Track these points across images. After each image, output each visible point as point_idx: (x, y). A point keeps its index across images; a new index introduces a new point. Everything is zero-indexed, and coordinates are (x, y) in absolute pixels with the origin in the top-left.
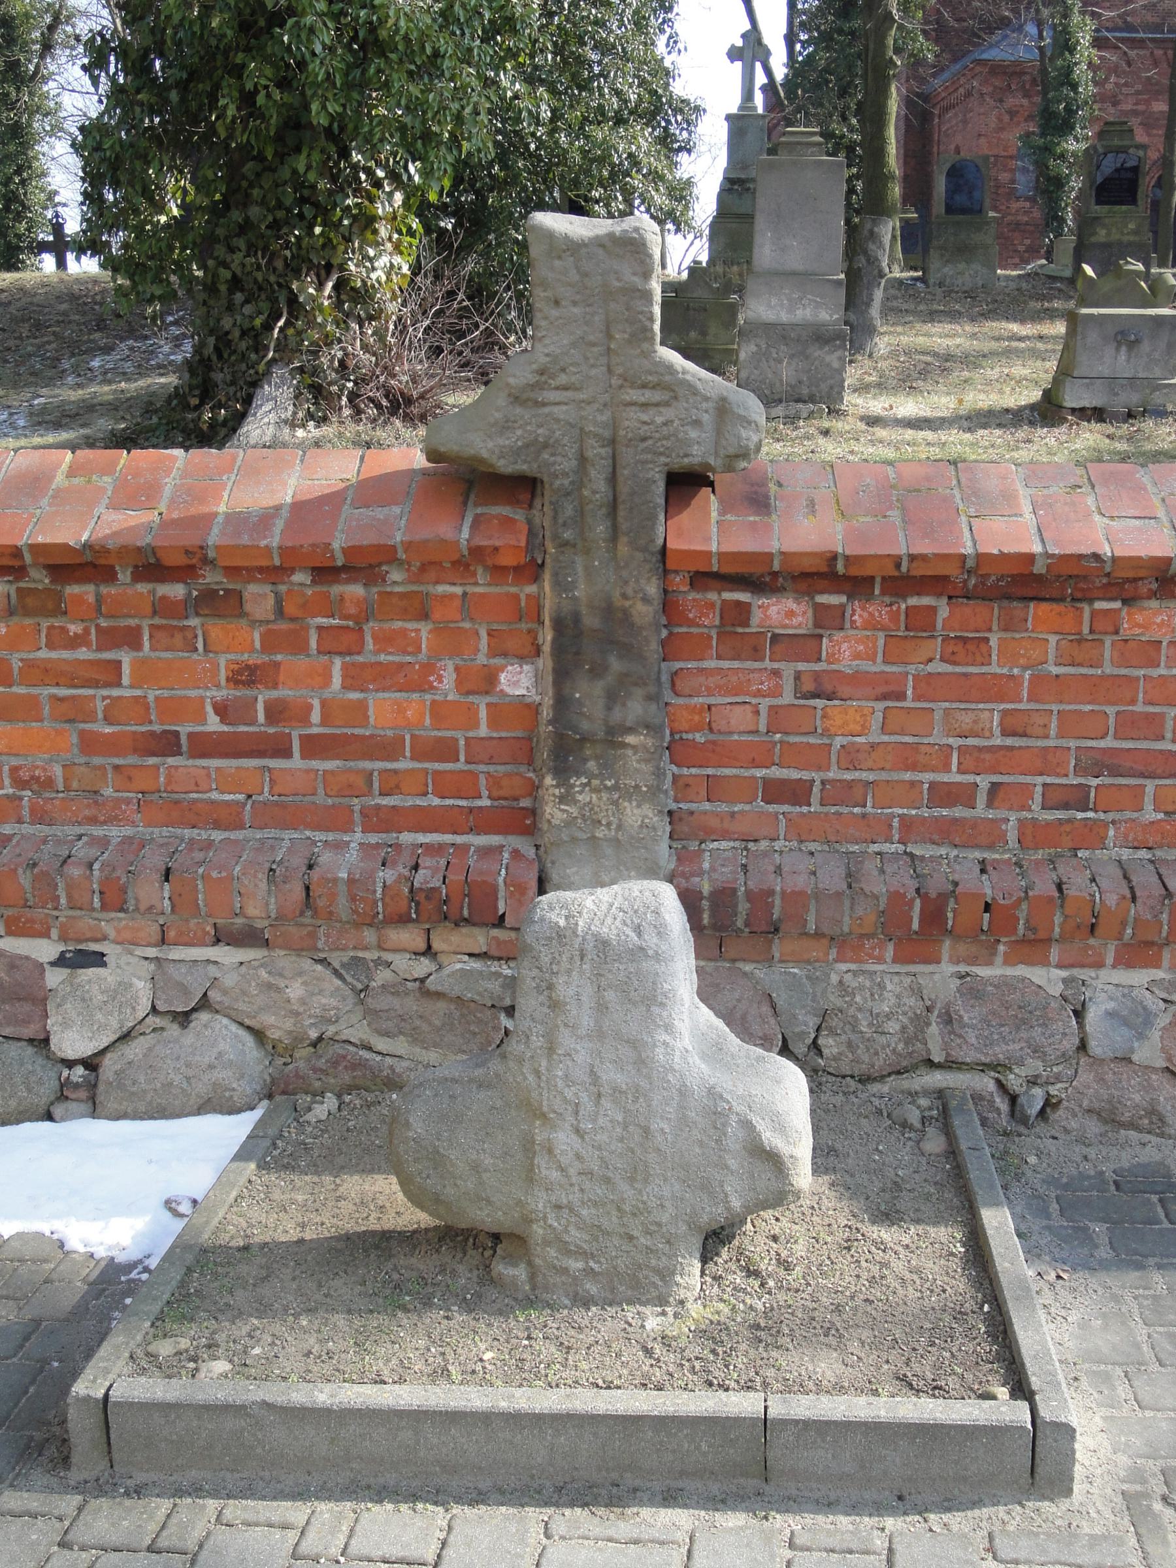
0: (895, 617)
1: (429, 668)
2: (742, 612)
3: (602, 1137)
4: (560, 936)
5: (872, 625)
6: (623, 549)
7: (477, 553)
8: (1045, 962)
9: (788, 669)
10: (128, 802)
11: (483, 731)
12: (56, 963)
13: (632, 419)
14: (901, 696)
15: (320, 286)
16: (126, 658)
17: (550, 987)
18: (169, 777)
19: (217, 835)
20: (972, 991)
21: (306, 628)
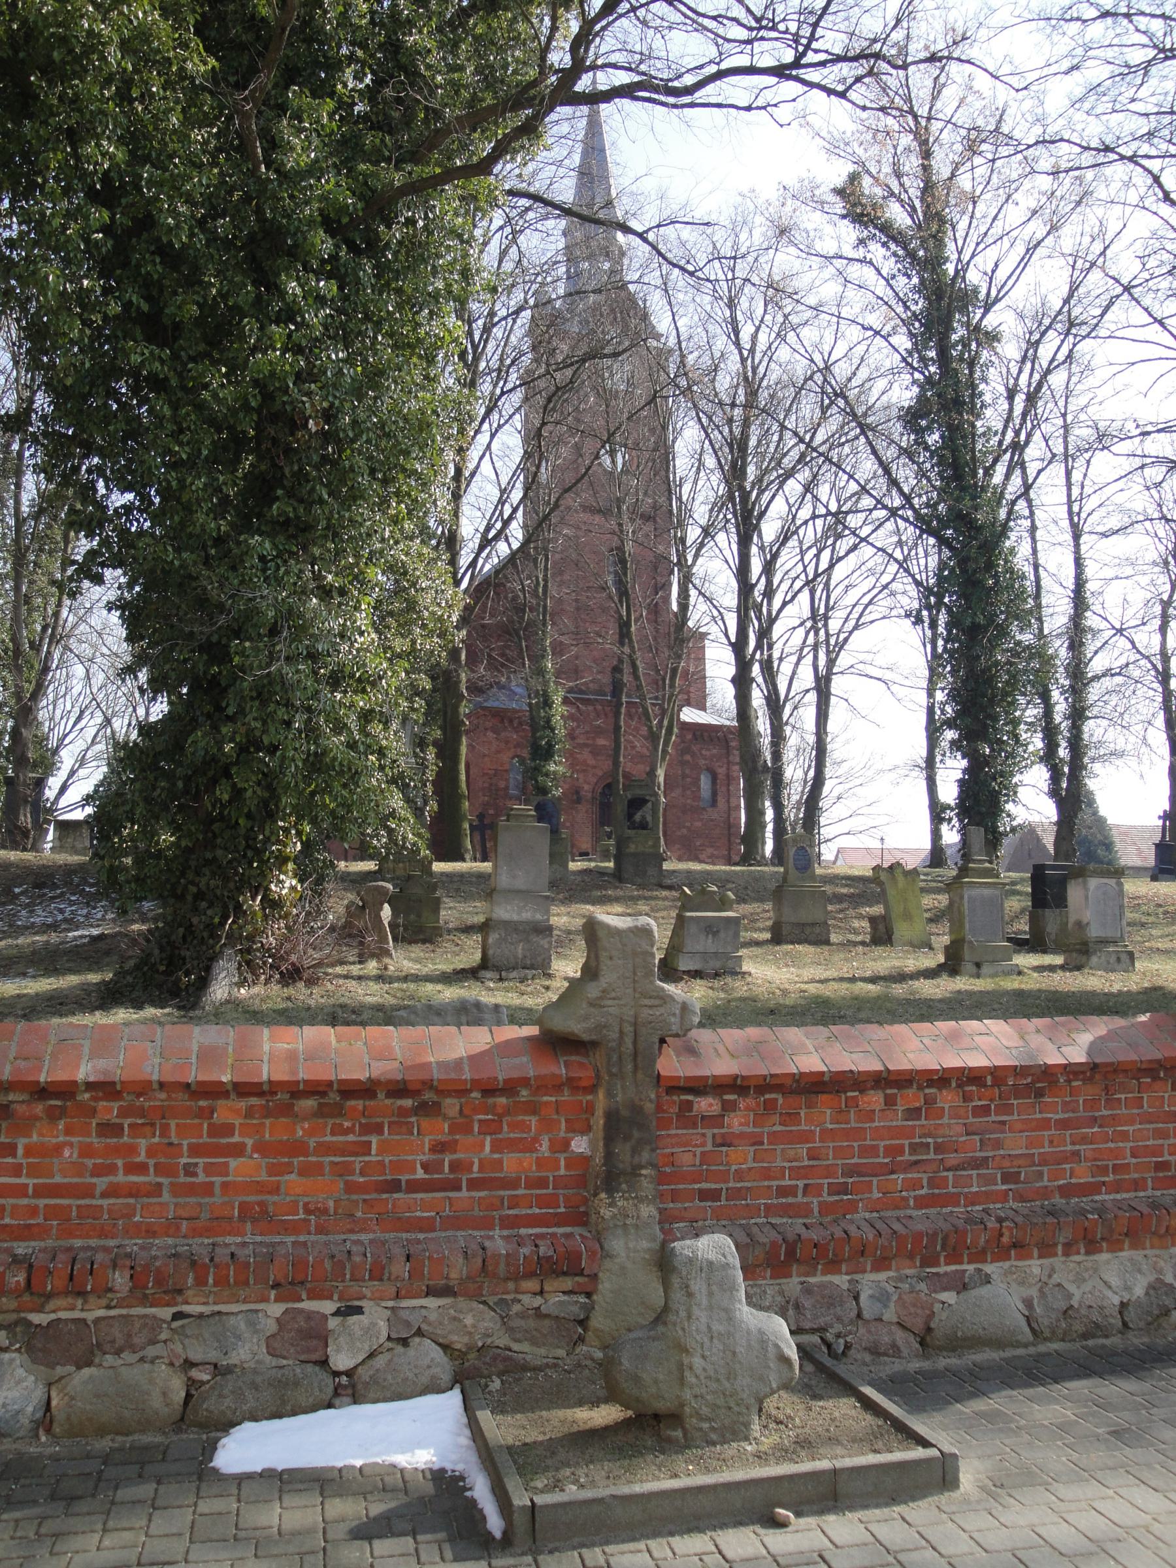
0: (758, 1104)
1: (536, 1140)
2: (689, 1105)
3: (714, 1358)
4: (691, 1261)
5: (748, 1109)
6: (640, 1076)
7: (570, 1080)
8: (839, 1272)
9: (709, 1133)
10: (371, 1219)
11: (562, 1172)
12: (335, 1314)
13: (645, 1013)
14: (762, 1143)
15: (254, 900)
16: (374, 1140)
17: (687, 1287)
18: (394, 1206)
19: (421, 1236)
20: (808, 1290)
21: (472, 1121)
